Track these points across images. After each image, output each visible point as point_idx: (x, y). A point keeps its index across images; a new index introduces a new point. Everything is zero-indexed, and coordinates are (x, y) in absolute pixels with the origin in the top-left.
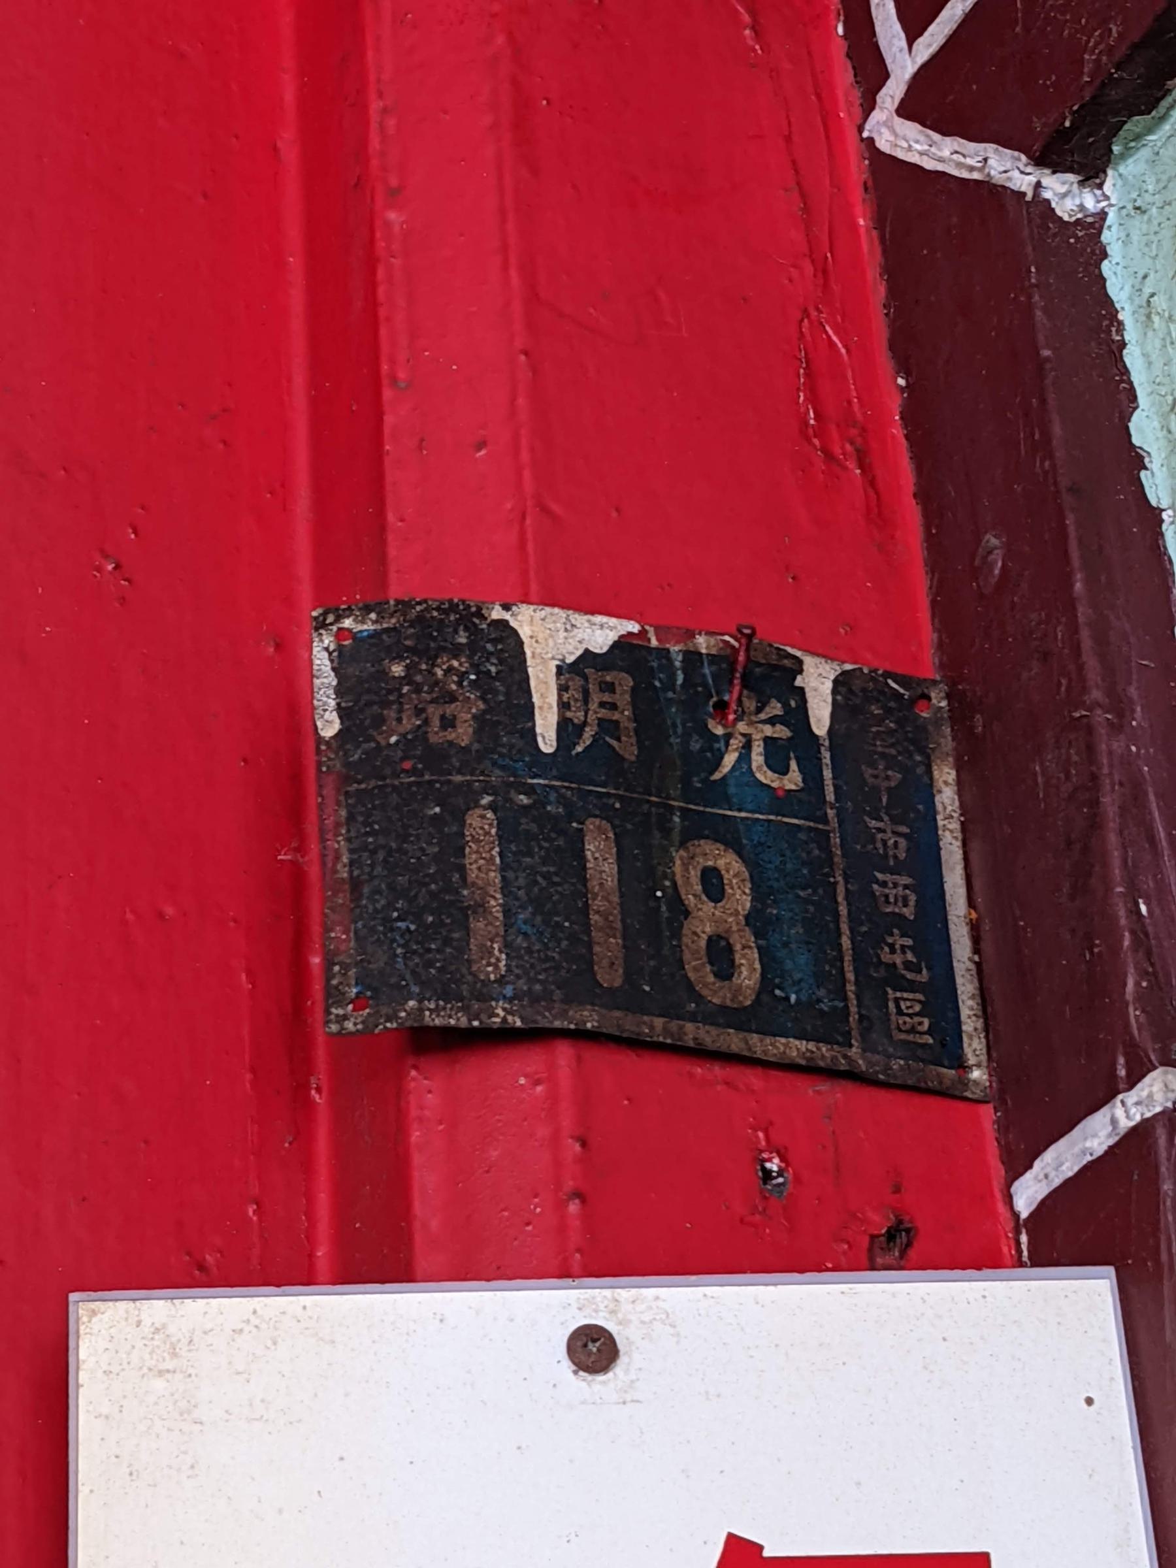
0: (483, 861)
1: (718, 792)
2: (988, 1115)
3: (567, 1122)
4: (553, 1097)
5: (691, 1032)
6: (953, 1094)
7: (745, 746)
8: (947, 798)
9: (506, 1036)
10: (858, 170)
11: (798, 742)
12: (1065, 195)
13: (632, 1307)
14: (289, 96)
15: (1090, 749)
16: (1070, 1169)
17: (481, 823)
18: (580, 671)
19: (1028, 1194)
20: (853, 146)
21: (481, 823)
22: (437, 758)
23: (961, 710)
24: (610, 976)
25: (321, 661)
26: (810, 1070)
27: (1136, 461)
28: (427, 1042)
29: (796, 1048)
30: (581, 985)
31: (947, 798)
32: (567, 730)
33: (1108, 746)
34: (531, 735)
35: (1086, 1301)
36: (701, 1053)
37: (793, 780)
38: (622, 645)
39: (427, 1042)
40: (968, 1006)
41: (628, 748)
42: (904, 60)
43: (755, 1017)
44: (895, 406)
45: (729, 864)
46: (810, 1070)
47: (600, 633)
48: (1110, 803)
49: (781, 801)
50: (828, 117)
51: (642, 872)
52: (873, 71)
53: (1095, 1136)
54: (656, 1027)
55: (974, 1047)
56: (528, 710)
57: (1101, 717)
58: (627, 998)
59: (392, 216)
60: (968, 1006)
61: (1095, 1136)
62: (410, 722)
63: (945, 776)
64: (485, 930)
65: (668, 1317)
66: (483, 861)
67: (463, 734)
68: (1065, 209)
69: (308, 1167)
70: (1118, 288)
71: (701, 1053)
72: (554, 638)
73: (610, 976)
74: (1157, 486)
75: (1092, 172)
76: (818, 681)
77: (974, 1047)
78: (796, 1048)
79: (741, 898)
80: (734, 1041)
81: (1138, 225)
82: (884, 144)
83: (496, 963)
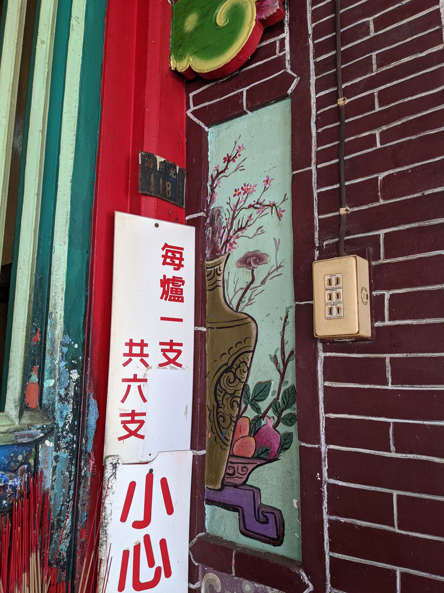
0: (152, 180)
1: (169, 177)
2: (184, 210)
3: (156, 205)
4: (155, 202)
5: (166, 199)
6: (182, 208)
7: (172, 173)
8: (185, 181)
9: (153, 196)
10: (185, 116)
11: (176, 174)
12: (206, 129)
13: (162, 223)
14: (133, 88)
15: (201, 183)
16: (192, 217)
17: (152, 176)
18: (161, 163)
19: (187, 218)
20: (185, 114)
21: (152, 176)
22: (149, 169)
23: (187, 173)
24: (161, 193)
25: (140, 156)
26: (174, 204)
27: (208, 156)
28: (146, 195)
29: (173, 202)
30: (159, 193)
31: (185, 181)
32: (160, 168)
33: (203, 183)
34: (157, 168)
35: (192, 230)
36: (167, 201)
37: (175, 177)
38: (164, 161)
39: (146, 195)
40: (184, 201)
41: (164, 171)
42: (192, 108)
43: (169, 198)
44: (185, 141)
45: (170, 184)
46: (174, 204)
47: (163, 160)
48: (202, 188)
49: (174, 179)
50: (183, 111)
51: (164, 183)
52: (189, 108)
53: (195, 216)
54: (163, 198)
55: (184, 204)
56: (157, 166)
57: (203, 180)
58: (162, 195)
59: (147, 110)
60: (184, 201)
61: (195, 216)
62: (147, 164)
63: (185, 179)
64: (152, 186)
65: (163, 224)
66: (152, 180)
67: (152, 167)
68: (206, 130)
69: (128, 201)
70: (209, 140)
71: (167, 201)
72: (160, 159)
73: (161, 193)
74: (209, 159)
75: (209, 128)
76: (178, 168)
77: (184, 204)
78: (173, 202)
79: (170, 187)
80: (169, 200)
81: (212, 134)
82: (188, 115)
83: (153, 190)
